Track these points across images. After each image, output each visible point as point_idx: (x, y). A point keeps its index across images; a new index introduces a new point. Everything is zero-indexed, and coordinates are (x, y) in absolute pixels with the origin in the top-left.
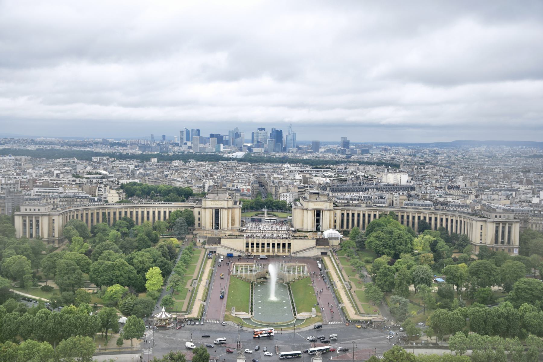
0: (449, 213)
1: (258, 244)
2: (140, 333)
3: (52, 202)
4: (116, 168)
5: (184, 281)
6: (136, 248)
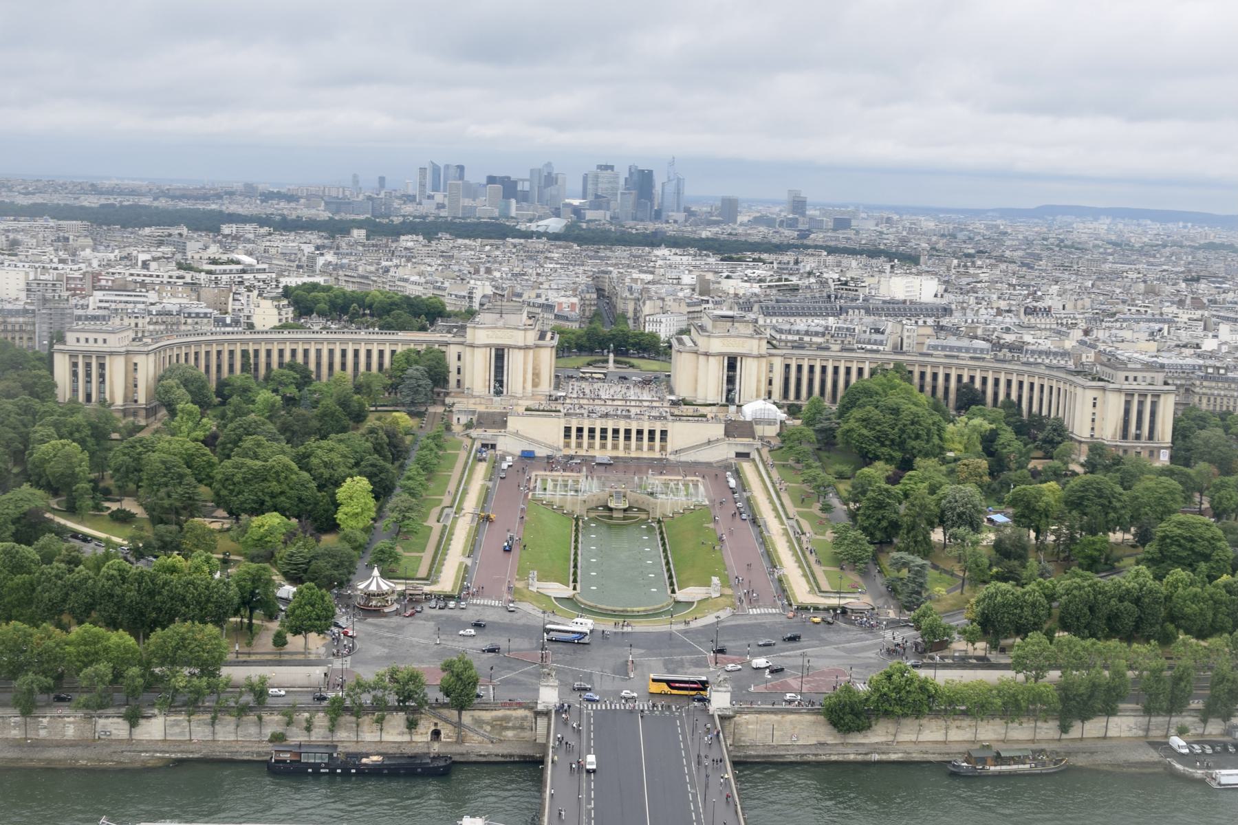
0: (1025, 368)
1: (592, 431)
2: (323, 622)
3: (133, 325)
4: (273, 251)
5: (424, 510)
6: (315, 433)
